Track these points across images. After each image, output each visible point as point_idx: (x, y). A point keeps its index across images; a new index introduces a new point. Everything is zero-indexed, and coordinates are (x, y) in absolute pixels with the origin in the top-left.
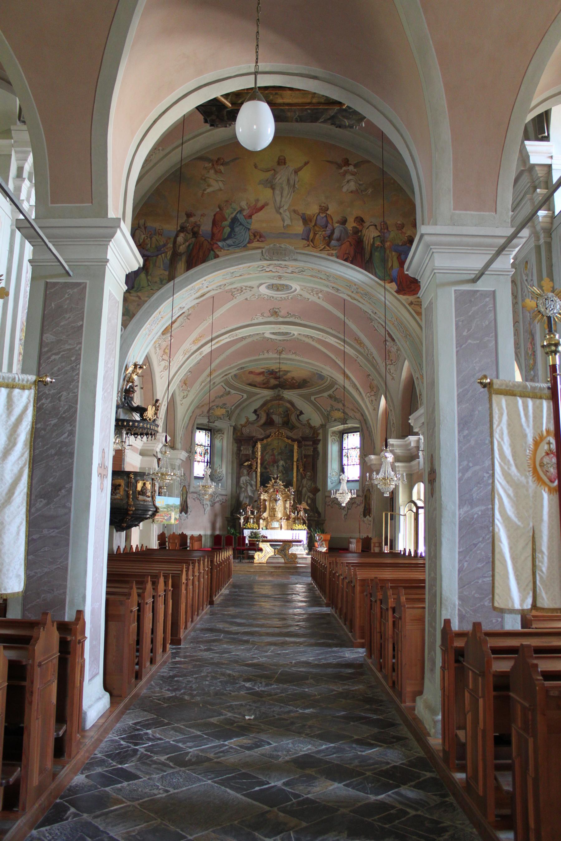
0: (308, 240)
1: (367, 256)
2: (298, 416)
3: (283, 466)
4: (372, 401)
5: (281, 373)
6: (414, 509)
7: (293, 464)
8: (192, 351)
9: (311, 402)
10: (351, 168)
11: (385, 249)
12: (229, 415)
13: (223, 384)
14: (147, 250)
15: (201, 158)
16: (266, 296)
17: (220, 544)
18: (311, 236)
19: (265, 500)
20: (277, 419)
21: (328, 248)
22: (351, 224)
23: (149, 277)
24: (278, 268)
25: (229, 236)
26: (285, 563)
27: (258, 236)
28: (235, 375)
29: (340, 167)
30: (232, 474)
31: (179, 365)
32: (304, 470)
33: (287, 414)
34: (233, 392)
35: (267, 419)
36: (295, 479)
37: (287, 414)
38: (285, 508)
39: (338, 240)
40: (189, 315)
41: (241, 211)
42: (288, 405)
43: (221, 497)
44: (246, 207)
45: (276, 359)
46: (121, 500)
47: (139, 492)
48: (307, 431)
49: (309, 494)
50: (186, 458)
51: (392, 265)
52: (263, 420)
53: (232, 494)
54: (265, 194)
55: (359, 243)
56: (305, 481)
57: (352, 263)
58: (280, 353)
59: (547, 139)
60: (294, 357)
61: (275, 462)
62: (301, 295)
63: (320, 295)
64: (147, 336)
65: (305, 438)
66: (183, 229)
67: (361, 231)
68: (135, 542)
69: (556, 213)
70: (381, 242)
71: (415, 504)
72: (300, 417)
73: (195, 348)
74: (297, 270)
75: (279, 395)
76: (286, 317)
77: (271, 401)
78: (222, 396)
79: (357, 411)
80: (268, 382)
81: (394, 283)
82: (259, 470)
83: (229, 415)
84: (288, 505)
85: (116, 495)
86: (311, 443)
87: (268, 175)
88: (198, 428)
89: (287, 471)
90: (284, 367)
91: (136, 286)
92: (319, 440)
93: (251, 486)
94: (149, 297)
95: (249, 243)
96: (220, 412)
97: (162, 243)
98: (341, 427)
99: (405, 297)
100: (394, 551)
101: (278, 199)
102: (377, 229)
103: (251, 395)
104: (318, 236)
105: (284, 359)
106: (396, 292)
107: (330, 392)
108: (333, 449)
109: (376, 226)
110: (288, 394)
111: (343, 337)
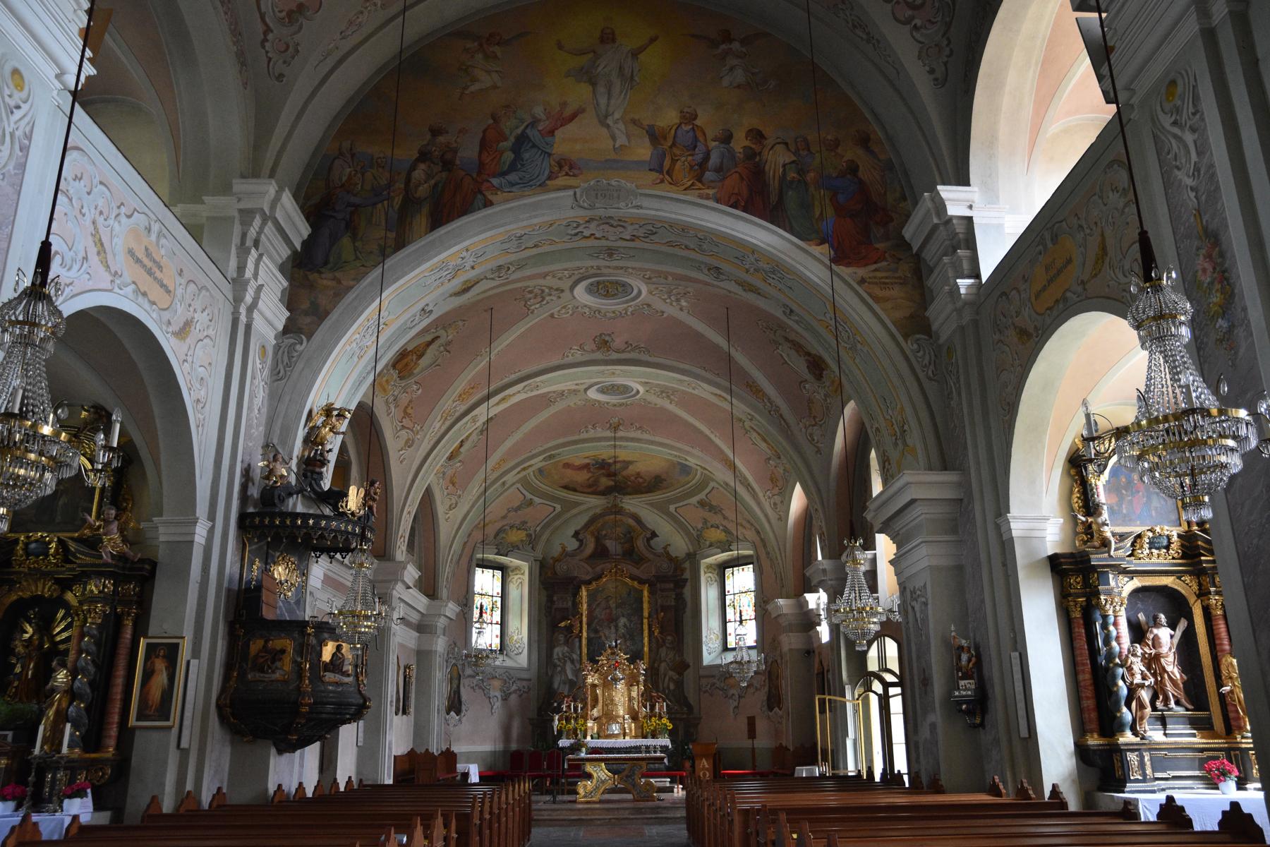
0: (661, 172)
1: (774, 198)
2: (648, 540)
3: (625, 626)
4: (775, 504)
5: (618, 466)
7: (642, 624)
8: (457, 414)
10: (736, 46)
12: (532, 541)
13: (519, 485)
14: (355, 195)
16: (587, 310)
18: (667, 163)
19: (594, 686)
20: (611, 545)
22: (740, 143)
24: (606, 227)
25: (512, 168)
26: (634, 800)
27: (567, 166)
28: (540, 471)
30: (539, 641)
31: (435, 439)
32: (660, 633)
34: (537, 500)
35: (596, 548)
36: (646, 649)
37: (629, 537)
38: (630, 699)
39: (718, 170)
40: (449, 343)
41: (534, 123)
42: (631, 522)
43: (519, 684)
44: (543, 117)
46: (285, 682)
47: (326, 664)
48: (665, 566)
49: (671, 673)
50: (458, 615)
52: (590, 547)
53: (539, 677)
54: (579, 93)
55: (756, 174)
56: (663, 652)
58: (616, 429)
59: (967, 183)
60: (638, 434)
61: (612, 620)
62: (649, 305)
64: (356, 359)
65: (661, 578)
66: (424, 156)
68: (346, 770)
69: (984, 280)
73: (463, 408)
74: (641, 233)
75: (616, 506)
76: (623, 351)
78: (517, 509)
79: (748, 525)
80: (596, 483)
81: (827, 245)
82: (585, 634)
84: (634, 694)
85: (273, 672)
86: (672, 585)
88: (479, 566)
90: (623, 455)
93: (572, 662)
94: (358, 279)
95: (549, 178)
96: (515, 536)
97: (384, 182)
99: (850, 270)
100: (841, 773)
101: (603, 101)
103: (568, 506)
105: (622, 439)
107: (702, 496)
108: (709, 595)
109: (786, 144)
110: (632, 504)
111: (728, 384)
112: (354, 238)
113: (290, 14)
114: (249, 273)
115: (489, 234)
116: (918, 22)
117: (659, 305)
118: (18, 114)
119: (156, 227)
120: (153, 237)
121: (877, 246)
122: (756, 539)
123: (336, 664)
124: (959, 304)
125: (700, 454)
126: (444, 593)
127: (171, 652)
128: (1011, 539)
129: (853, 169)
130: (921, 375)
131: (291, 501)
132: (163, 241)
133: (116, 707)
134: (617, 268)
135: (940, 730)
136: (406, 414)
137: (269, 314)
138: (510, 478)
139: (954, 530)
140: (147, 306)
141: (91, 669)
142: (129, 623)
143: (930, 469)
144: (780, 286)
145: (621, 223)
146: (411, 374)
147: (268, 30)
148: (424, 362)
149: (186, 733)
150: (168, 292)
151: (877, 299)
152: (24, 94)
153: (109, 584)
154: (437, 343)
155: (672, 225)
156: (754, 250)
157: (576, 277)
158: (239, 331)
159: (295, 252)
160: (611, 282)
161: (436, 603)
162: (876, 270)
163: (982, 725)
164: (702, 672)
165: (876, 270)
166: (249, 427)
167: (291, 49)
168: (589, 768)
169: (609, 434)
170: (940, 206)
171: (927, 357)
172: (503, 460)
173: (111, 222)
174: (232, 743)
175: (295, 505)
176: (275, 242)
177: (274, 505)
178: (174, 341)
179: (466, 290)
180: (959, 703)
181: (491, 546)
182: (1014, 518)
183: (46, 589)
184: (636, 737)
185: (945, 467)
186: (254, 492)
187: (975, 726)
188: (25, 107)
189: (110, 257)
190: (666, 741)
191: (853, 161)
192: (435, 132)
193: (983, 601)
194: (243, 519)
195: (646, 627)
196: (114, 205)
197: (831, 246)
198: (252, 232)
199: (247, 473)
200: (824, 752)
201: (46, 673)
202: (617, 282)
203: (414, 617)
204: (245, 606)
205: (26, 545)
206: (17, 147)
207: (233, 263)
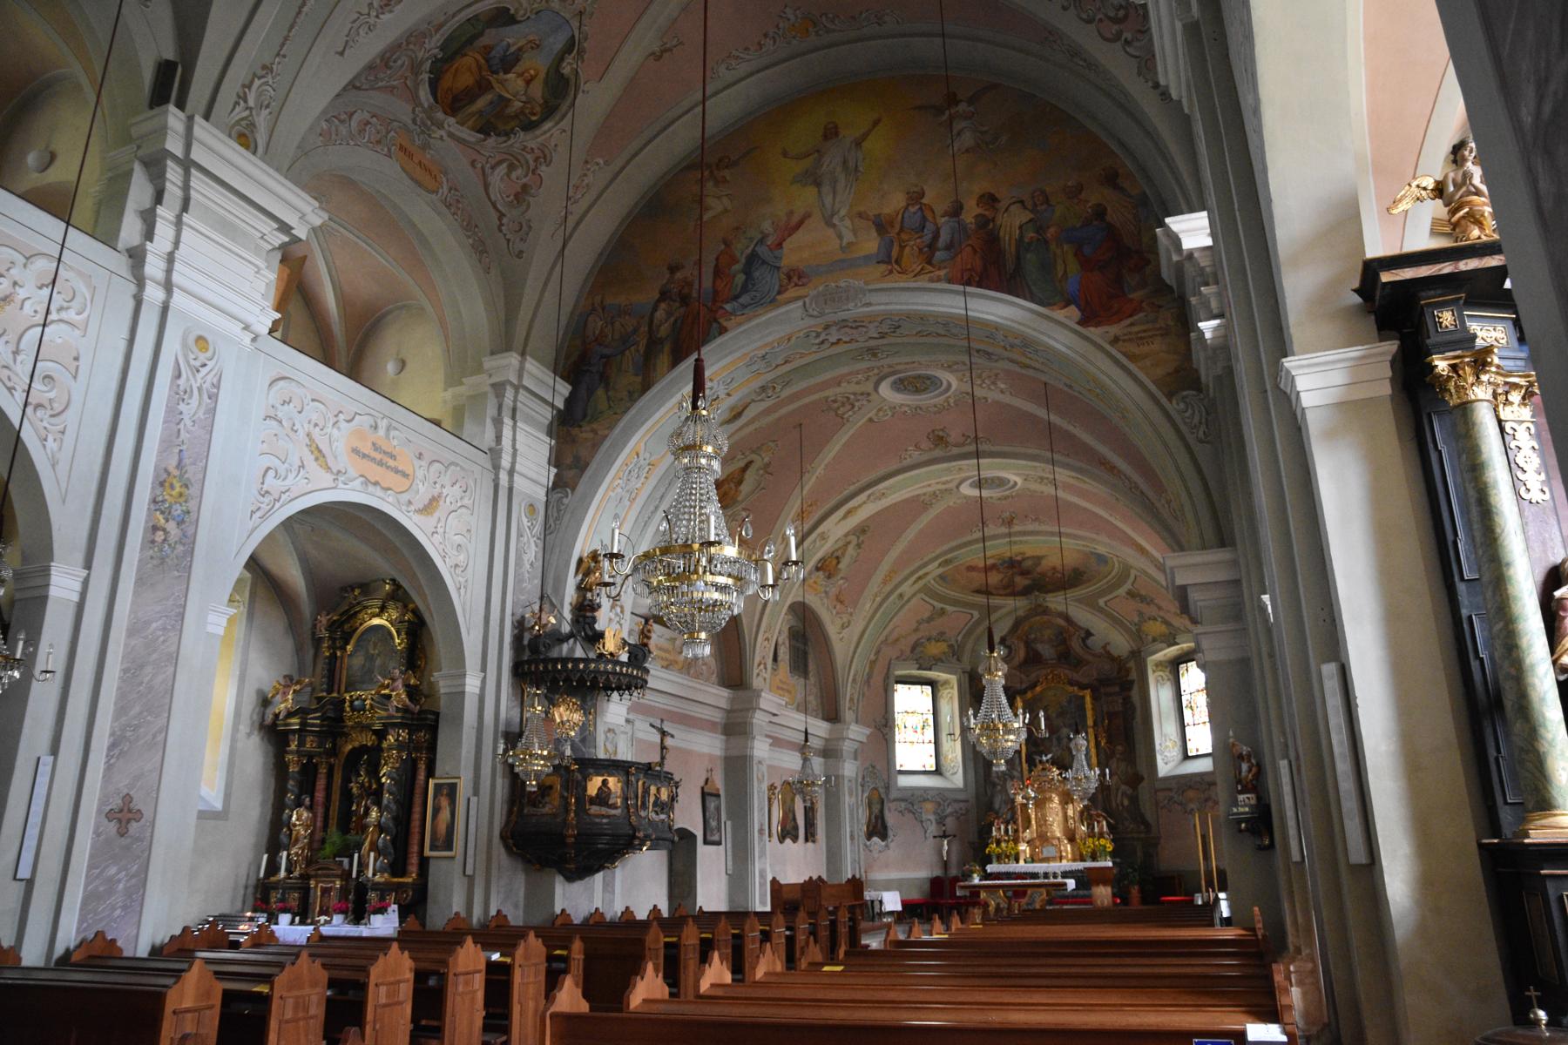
0: (889, 262)
2: (1084, 640)
9: (1101, 610)
10: (962, 107)
11: (1046, 242)
15: (689, 167)
18: (894, 254)
20: (1046, 651)
21: (930, 268)
25: (745, 289)
28: (942, 577)
29: (939, 111)
34: (949, 608)
35: (1027, 653)
39: (949, 247)
41: (761, 241)
42: (1062, 622)
43: (956, 806)
46: (555, 815)
47: (591, 798)
54: (805, 197)
55: (989, 239)
57: (979, 286)
58: (1010, 523)
66: (664, 295)
67: (993, 220)
70: (1037, 232)
72: (1089, 642)
74: (885, 328)
76: (963, 445)
77: (1027, 617)
78: (930, 619)
86: (1117, 689)
87: (807, 163)
91: (589, 412)
92: (1132, 682)
94: (611, 428)
95: (779, 293)
96: (935, 649)
97: (630, 329)
98: (1172, 651)
101: (828, 200)
102: (1025, 208)
104: (907, 250)
106: (1078, 323)
107: (1127, 586)
108: (1160, 696)
109: (1022, 202)
110: (1055, 602)
112: (607, 389)
113: (517, 196)
116: (1128, 35)
118: (204, 371)
119: (383, 424)
120: (381, 432)
123: (603, 797)
125: (1107, 540)
126: (848, 715)
127: (452, 790)
129: (1100, 212)
130: (1190, 438)
131: (565, 647)
132: (393, 433)
133: (415, 839)
138: (906, 588)
140: (379, 492)
141: (393, 806)
142: (422, 767)
143: (1204, 548)
145: (857, 324)
146: (735, 501)
147: (502, 215)
148: (745, 488)
149: (470, 861)
150: (405, 475)
151: (1132, 357)
152: (209, 354)
157: (874, 379)
158: (501, 494)
161: (838, 726)
162: (1132, 324)
163: (1272, 845)
164: (1158, 785)
165: (1132, 324)
169: (1004, 530)
170: (1175, 240)
174: (526, 871)
175: (572, 650)
178: (417, 518)
179: (738, 415)
180: (1239, 822)
181: (919, 662)
183: (368, 740)
184: (1074, 860)
185: (1222, 543)
188: (210, 364)
191: (1099, 205)
192: (673, 269)
199: (520, 625)
200: (1209, 873)
202: (919, 376)
205: (352, 702)
206: (205, 396)
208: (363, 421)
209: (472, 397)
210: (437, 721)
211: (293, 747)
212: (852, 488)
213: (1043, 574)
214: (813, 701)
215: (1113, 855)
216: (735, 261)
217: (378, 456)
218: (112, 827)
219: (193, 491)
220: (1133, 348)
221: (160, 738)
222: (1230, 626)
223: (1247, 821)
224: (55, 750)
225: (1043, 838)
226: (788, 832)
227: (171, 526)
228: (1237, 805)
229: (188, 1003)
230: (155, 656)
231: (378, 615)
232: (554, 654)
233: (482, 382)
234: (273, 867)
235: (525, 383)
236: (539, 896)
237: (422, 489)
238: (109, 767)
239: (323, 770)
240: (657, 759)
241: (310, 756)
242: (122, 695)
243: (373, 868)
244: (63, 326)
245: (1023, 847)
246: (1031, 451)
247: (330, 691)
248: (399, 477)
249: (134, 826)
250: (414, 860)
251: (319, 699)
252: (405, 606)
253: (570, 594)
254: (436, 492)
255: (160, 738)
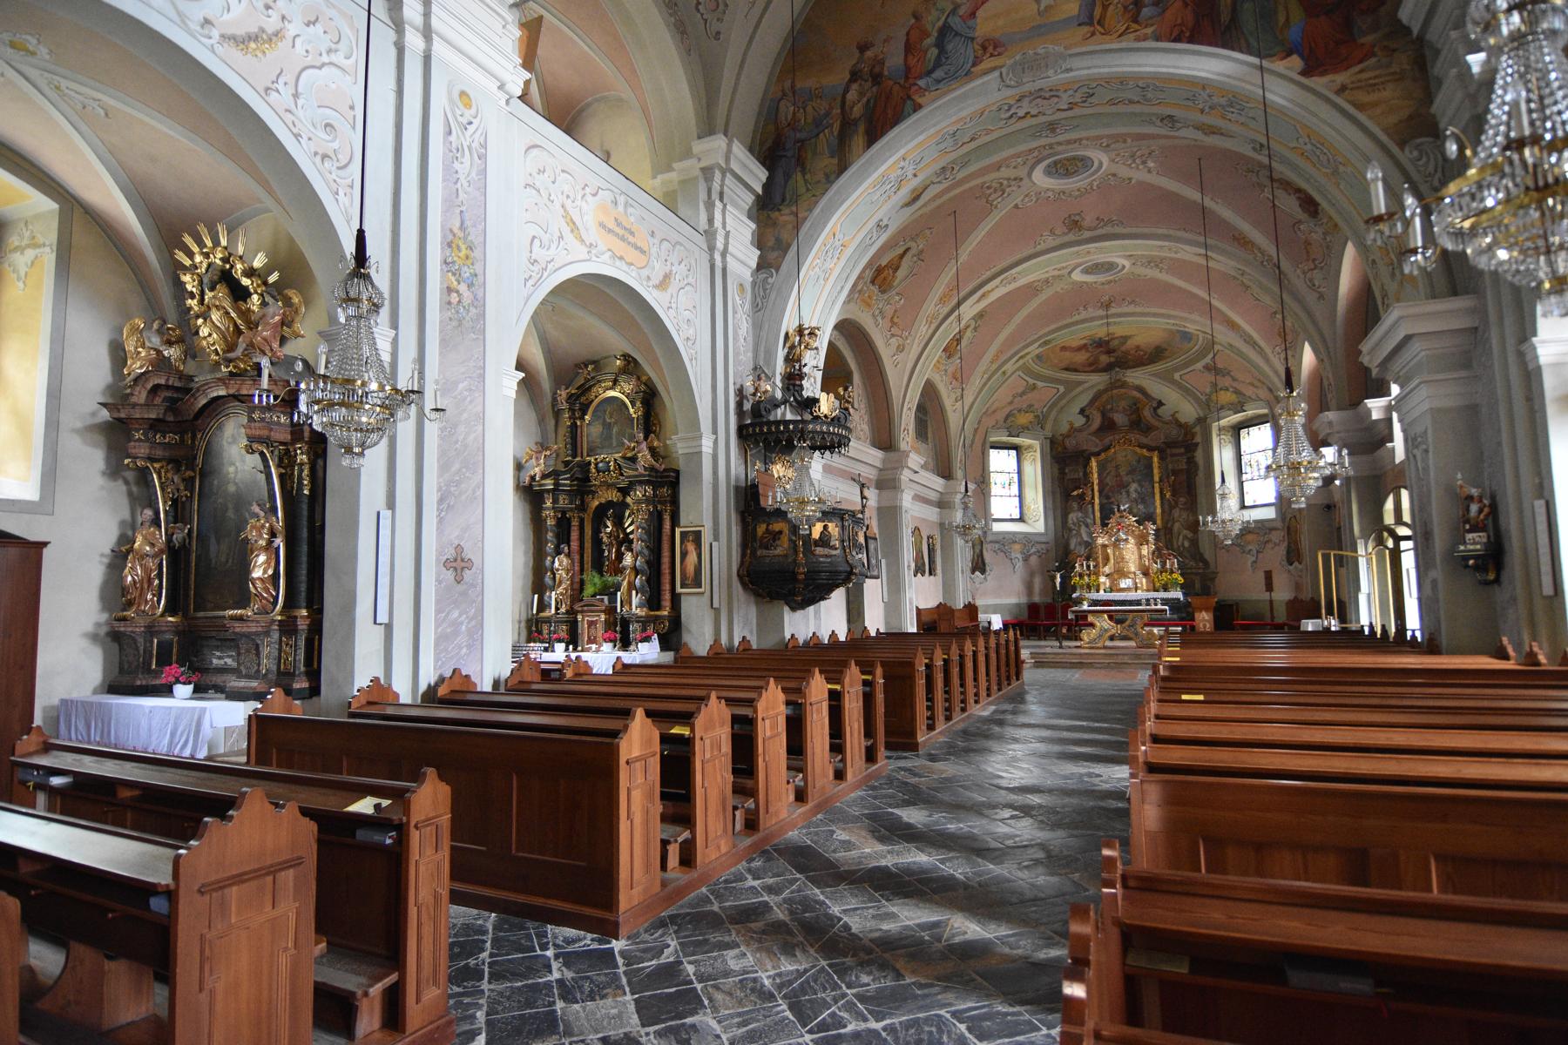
0: (1091, 24)
1: (1225, 17)
2: (1155, 409)
6: (1390, 543)
9: (1174, 382)
12: (1040, 421)
17: (1054, 618)
18: (1097, 12)
19: (1104, 546)
20: (1120, 419)
21: (1136, 26)
23: (808, 176)
25: (938, 64)
28: (1038, 356)
33: (1135, 410)
34: (1040, 384)
36: (1159, 511)
37: (1135, 410)
38: (1141, 557)
42: (1138, 395)
45: (1101, 318)
46: (786, 556)
51: (1287, 19)
52: (1097, 422)
56: (1176, 513)
57: (1191, 41)
58: (1108, 306)
60: (1131, 309)
63: (1151, 164)
65: (1170, 444)
66: (855, 76)
71: (1393, 534)
72: (1160, 411)
73: (946, 310)
77: (1106, 390)
78: (1023, 393)
82: (1097, 501)
83: (1040, 421)
89: (1145, 498)
90: (1119, 331)
92: (1197, 445)
94: (811, 210)
95: (974, 65)
96: (1023, 419)
100: (1353, 627)
103: (1071, 386)
107: (1208, 360)
108: (1223, 457)
110: (1136, 377)
114: (718, 223)
115: (921, 138)
117: (1124, 172)
118: (471, 129)
119: (622, 199)
120: (621, 208)
121: (1363, 40)
122: (1270, 397)
123: (824, 540)
124: (1472, 89)
127: (697, 537)
128: (1539, 368)
131: (779, 411)
132: (630, 210)
133: (666, 579)
134: (1069, 142)
135: (1440, 585)
136: (893, 324)
137: (739, 255)
138: (1009, 367)
139: (1467, 365)
140: (625, 267)
141: (646, 552)
144: (1242, 119)
145: (1054, 93)
146: (890, 287)
148: (901, 273)
150: (643, 252)
151: (1360, 107)
153: (649, 490)
154: (909, 255)
155: (1108, 81)
156: (1204, 84)
157: (1029, 163)
158: (717, 274)
159: (758, 196)
160: (1067, 159)
162: (1361, 71)
163: (1497, 581)
165: (1361, 71)
166: (736, 354)
167: (721, 7)
168: (1090, 618)
169: (1101, 312)
171: (1432, 162)
172: (1001, 352)
173: (578, 203)
174: (757, 603)
175: (784, 414)
176: (738, 191)
177: (761, 416)
178: (656, 293)
180: (1466, 558)
181: (1007, 429)
182: (1543, 342)
183: (614, 496)
185: (1454, 292)
186: (747, 406)
187: (1487, 583)
189: (582, 231)
190: (1178, 594)
193: (1499, 444)
194: (741, 429)
195: (1157, 491)
196: (578, 187)
197: (1301, 56)
198: (716, 186)
199: (740, 392)
201: (620, 556)
202: (1074, 158)
203: (933, 496)
204: (749, 501)
207: (703, 217)
208: (606, 196)
209: (683, 182)
210: (677, 478)
211: (549, 504)
212: (989, 274)
213: (1127, 353)
214: (932, 464)
215: (1183, 587)
216: (926, 34)
217: (621, 232)
218: (450, 575)
219: (477, 253)
220: (1364, 97)
221: (479, 493)
222: (1463, 373)
223: (1476, 557)
224: (391, 504)
225: (1121, 573)
226: (919, 570)
227: (463, 288)
228: (1465, 543)
229: (636, 753)
230: (465, 415)
231: (611, 388)
232: (772, 418)
233: (691, 166)
234: (543, 606)
235: (734, 166)
236: (769, 624)
237: (657, 266)
238: (441, 521)
239: (575, 523)
240: (859, 507)
241: (564, 513)
242: (442, 453)
243: (636, 606)
244: (334, 69)
245: (1102, 579)
246: (1160, 231)
247: (574, 456)
248: (637, 253)
249: (467, 574)
250: (667, 596)
251: (566, 464)
252: (639, 378)
253: (780, 367)
254: (667, 269)
255: (479, 493)
